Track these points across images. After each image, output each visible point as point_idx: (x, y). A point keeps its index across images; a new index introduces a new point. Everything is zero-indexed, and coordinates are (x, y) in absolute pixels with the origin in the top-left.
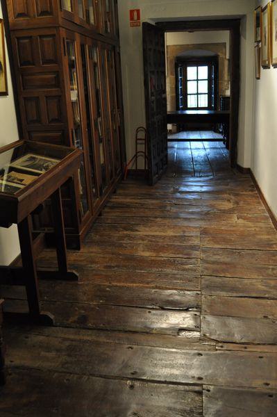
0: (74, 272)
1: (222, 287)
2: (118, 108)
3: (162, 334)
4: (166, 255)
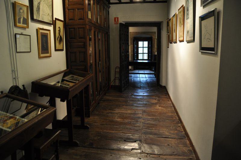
0: (88, 125)
1: (151, 133)
2: (108, 58)
3: (125, 150)
4: (127, 120)
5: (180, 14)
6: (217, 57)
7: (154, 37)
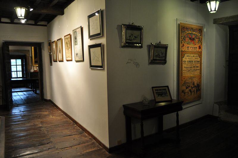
5: (67, 40)
6: (105, 71)
7: (27, 55)
